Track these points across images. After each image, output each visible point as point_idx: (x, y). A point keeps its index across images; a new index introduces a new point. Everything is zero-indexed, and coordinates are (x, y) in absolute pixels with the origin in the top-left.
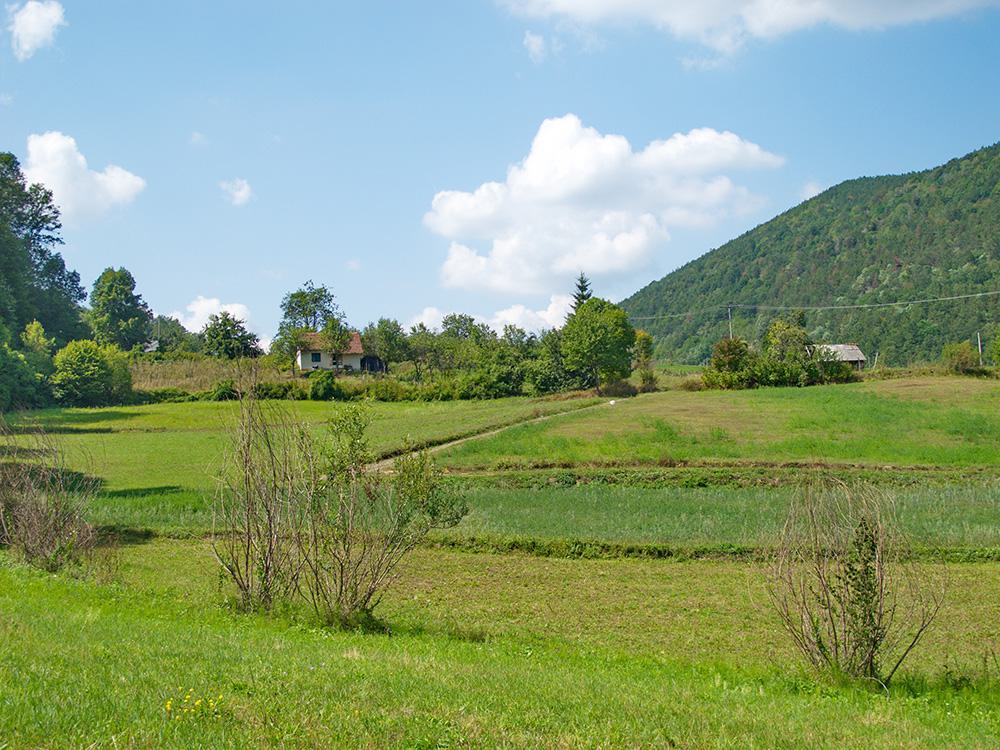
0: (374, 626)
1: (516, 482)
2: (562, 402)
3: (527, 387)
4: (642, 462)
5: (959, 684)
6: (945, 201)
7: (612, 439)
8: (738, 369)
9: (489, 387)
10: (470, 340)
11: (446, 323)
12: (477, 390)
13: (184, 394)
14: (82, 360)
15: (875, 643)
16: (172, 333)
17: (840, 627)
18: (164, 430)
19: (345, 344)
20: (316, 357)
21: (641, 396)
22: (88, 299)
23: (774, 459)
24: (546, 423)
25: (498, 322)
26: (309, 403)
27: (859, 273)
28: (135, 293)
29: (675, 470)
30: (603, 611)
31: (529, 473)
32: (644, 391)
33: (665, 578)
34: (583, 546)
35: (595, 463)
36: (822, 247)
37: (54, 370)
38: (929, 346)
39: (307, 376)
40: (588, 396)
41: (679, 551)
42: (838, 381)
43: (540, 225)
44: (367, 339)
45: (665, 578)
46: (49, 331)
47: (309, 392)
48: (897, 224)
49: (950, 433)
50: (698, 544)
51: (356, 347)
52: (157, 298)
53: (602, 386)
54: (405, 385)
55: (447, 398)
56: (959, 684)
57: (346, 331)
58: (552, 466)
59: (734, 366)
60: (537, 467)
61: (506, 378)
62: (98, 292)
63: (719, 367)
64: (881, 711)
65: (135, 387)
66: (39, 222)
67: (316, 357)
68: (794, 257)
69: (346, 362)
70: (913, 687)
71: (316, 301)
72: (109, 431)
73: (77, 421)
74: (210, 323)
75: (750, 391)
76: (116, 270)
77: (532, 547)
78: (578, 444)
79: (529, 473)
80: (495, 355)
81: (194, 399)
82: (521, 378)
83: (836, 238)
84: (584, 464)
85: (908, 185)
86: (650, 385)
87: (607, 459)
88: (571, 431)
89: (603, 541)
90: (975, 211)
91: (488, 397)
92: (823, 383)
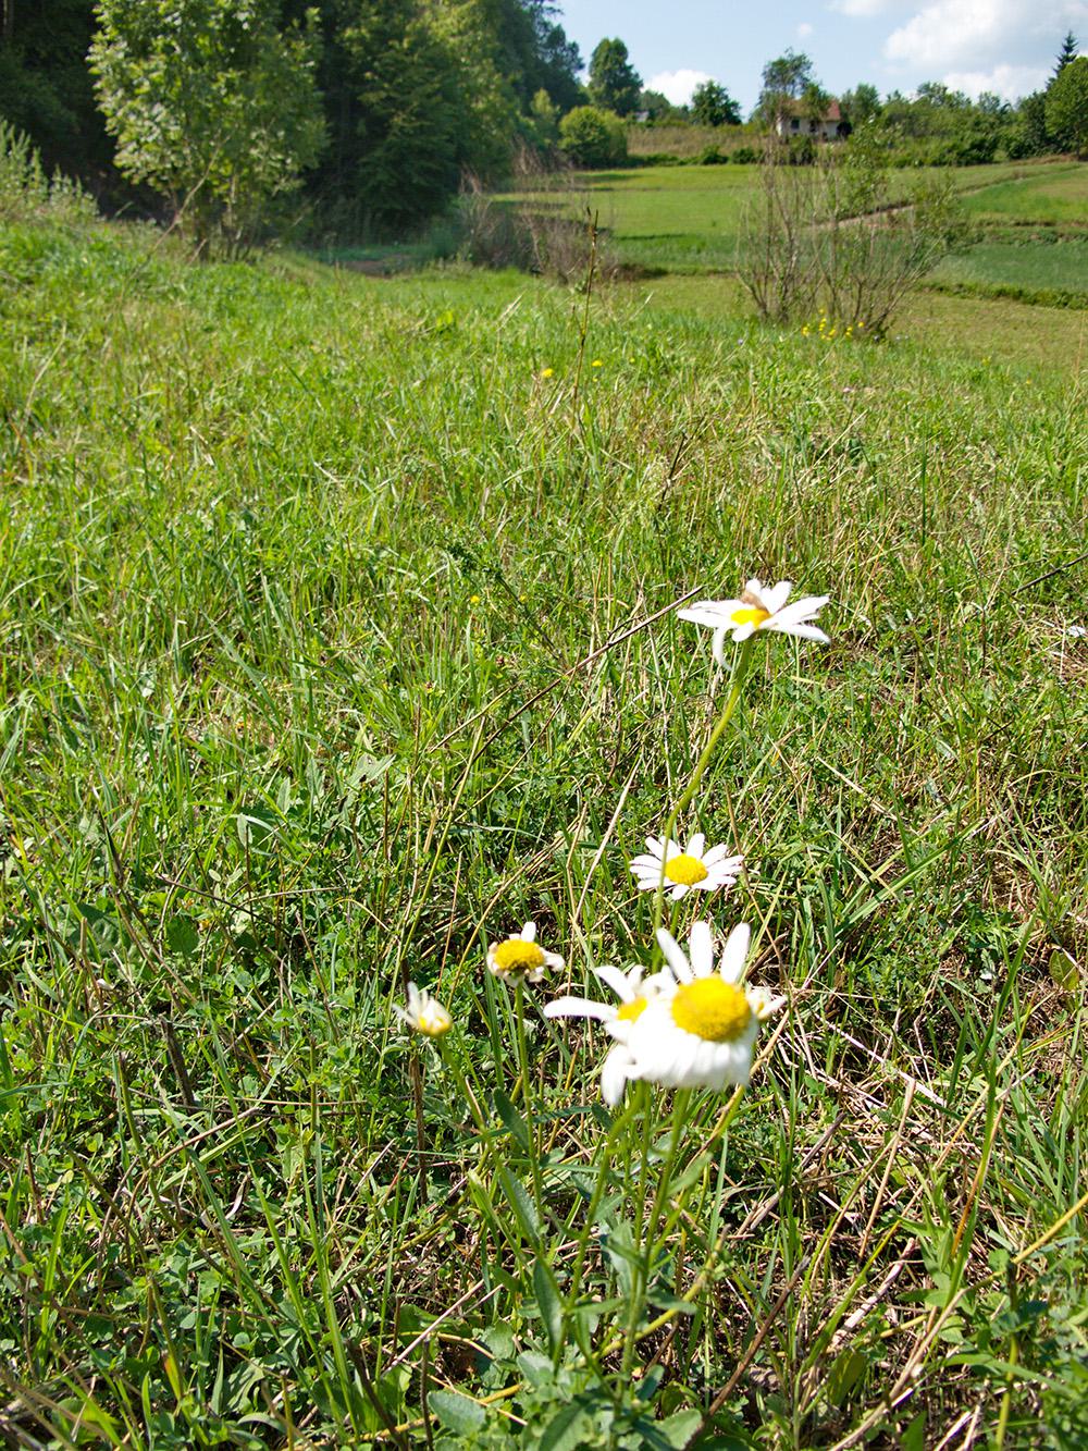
1: (998, 238)
3: (1000, 154)
9: (962, 154)
10: (944, 108)
11: (920, 92)
12: (948, 157)
13: (674, 159)
14: (584, 125)
16: (658, 106)
18: (658, 189)
19: (823, 110)
22: (587, 69)
24: (1027, 184)
25: (971, 87)
31: (1011, 230)
34: (1070, 297)
37: (560, 136)
40: (1067, 161)
44: (845, 107)
46: (554, 102)
51: (834, 114)
58: (1033, 224)
60: (1018, 224)
61: (979, 146)
62: (595, 64)
65: (630, 152)
67: (795, 124)
71: (796, 68)
72: (635, 177)
74: (697, 92)
77: (1018, 296)
79: (1011, 230)
80: (970, 121)
81: (682, 164)
82: (994, 146)
84: (1066, 222)
88: (1054, 191)
91: (959, 164)
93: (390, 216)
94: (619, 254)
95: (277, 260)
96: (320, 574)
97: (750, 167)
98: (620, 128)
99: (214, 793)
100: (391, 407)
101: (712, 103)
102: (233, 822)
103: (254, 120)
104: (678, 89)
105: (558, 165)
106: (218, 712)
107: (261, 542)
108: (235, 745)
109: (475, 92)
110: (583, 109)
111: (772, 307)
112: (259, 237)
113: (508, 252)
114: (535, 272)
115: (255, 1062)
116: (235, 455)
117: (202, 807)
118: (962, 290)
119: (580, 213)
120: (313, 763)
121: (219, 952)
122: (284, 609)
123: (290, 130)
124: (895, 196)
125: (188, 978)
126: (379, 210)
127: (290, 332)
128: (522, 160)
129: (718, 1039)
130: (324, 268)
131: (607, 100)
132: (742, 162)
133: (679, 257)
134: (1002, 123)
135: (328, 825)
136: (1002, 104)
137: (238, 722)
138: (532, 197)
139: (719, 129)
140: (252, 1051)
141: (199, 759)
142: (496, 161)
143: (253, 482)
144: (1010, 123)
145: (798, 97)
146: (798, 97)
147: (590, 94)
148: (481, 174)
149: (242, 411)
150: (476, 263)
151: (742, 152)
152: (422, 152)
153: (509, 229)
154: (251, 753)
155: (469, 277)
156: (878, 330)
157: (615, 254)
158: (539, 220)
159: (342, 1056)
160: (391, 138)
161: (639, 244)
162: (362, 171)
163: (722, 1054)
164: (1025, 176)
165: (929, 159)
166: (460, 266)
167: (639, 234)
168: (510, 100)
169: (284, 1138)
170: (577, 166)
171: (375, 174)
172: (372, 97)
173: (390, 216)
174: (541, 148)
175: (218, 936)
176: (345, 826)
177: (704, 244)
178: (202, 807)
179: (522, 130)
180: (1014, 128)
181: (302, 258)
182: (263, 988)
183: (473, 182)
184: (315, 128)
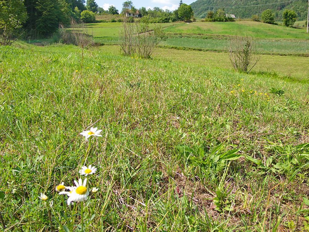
2: (178, 23)
3: (170, 21)
4: (195, 34)
8: (212, 18)
9: (163, 21)
10: (159, 12)
14: (86, 14)
15: (247, 65)
16: (102, 11)
18: (102, 27)
19: (136, 12)
20: (130, 14)
21: (193, 22)
22: (86, 3)
29: (201, 36)
34: (185, 48)
40: (183, 22)
41: (203, 50)
42: (231, 21)
44: (139, 11)
46: (79, 9)
49: (253, 32)
50: (207, 49)
51: (137, 13)
58: (178, 34)
59: (211, 17)
60: (175, 34)
61: (166, 19)
63: (208, 17)
67: (130, 14)
71: (129, 4)
75: (214, 22)
77: (176, 48)
81: (107, 22)
82: (169, 19)
86: (195, 20)
87: (188, 33)
88: (181, 28)
89: (189, 47)
91: (163, 23)
93: (43, 33)
94: (94, 41)
95: (17, 43)
96: (29, 118)
97: (121, 23)
98: (93, 15)
99: (7, 166)
100: (43, 79)
101: (113, 10)
102: (11, 171)
103: (10, 12)
104: (106, 8)
105: (80, 22)
106: (7, 149)
107: (15, 111)
108: (11, 156)
109: (62, 7)
110: (85, 11)
111: (127, 51)
112: (13, 38)
113: (70, 40)
114: (77, 45)
115: (19, 218)
116: (8, 92)
117: (5, 169)
118: (165, 47)
119: (86, 33)
120: (28, 158)
121: (10, 197)
122: (21, 125)
123: (18, 15)
124: (150, 29)
125: (3, 203)
126: (41, 32)
127: (20, 62)
128: (72, 22)
129: (82, 194)
130: (28, 44)
131: (90, 9)
132: (119, 22)
133: (107, 41)
134: (170, 15)
135: (31, 170)
136: (170, 11)
137: (12, 151)
138: (75, 29)
140: (17, 216)
141: (3, 159)
142: (67, 21)
143: (13, 98)
144: (172, 15)
145: (130, 9)
146: (130, 9)
147: (87, 8)
148: (63, 24)
149: (9, 81)
150: (63, 43)
152: (50, 19)
153: (71, 36)
154: (15, 157)
155: (62, 46)
156: (148, 55)
157: (94, 41)
158: (77, 34)
159: (34, 210)
160: (43, 16)
161: (99, 39)
162: (36, 23)
163: (83, 196)
164: (175, 25)
165: (157, 22)
166: (60, 44)
167: (98, 37)
168: (69, 9)
169: (24, 228)
170: (84, 23)
171: (40, 24)
172: (38, 7)
173: (43, 33)
174: (76, 19)
175: (9, 194)
176: (35, 170)
177: (112, 39)
178: (5, 169)
179: (72, 15)
180: (173, 16)
181: (23, 42)
182: (19, 203)
183: (62, 26)
184: (25, 15)
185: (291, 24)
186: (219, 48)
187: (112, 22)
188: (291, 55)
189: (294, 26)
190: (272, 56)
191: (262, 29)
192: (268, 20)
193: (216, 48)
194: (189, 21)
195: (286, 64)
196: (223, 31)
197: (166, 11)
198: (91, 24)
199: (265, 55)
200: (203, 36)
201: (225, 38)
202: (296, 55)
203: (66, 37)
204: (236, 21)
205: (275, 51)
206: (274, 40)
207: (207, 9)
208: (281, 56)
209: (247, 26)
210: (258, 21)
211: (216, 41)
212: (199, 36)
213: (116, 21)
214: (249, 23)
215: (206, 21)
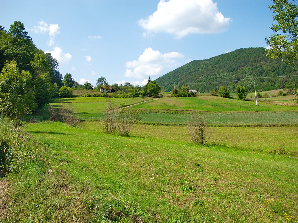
0: (128, 136)
1: (142, 113)
2: (147, 99)
3: (140, 95)
4: (162, 110)
5: (215, 145)
6: (211, 65)
7: (157, 106)
8: (177, 94)
9: (134, 95)
12: (131, 96)
13: (81, 96)
14: (64, 90)
15: (203, 139)
17: (198, 137)
18: (80, 102)
19: (109, 88)
20: (104, 90)
21: (161, 98)
23: (184, 110)
25: (135, 84)
26: (103, 98)
27: (196, 76)
28: (71, 78)
29: (169, 112)
30: (160, 134)
32: (161, 97)
33: (168, 129)
34: (155, 124)
35: (155, 110)
36: (189, 72)
38: (207, 90)
39: (102, 93)
40: (151, 98)
41: (170, 125)
42: (193, 96)
43: (143, 68)
44: (113, 86)
45: (168, 129)
47: (103, 96)
48: (202, 68)
49: (212, 106)
50: (173, 123)
52: (74, 78)
53: (154, 96)
54: (119, 95)
55: (126, 97)
56: (215, 145)
57: (109, 85)
59: (176, 93)
61: (137, 94)
63: (174, 93)
64: (204, 148)
65: (73, 95)
66: (55, 65)
67: (104, 90)
68: (185, 73)
69: (109, 91)
70: (208, 145)
71: (103, 80)
72: (70, 102)
73: (65, 100)
75: (179, 98)
76: (68, 74)
78: (151, 106)
80: (135, 90)
81: (83, 97)
82: (139, 94)
83: (192, 70)
85: (204, 62)
86: (162, 96)
87: (156, 109)
88: (150, 104)
89: (158, 123)
90: (215, 66)
92: (191, 96)
101: (88, 86)
110: (64, 87)
113: (58, 117)
114: (63, 122)
139: (89, 90)
147: (64, 83)
150: (52, 120)
151: (94, 95)
165: (128, 96)
185: (244, 98)
186: (182, 123)
187: (88, 97)
188: (242, 126)
189: (246, 99)
190: (226, 128)
191: (220, 102)
192: (225, 95)
193: (181, 122)
194: (157, 97)
195: (237, 135)
196: (187, 105)
197: (136, 86)
198: (69, 98)
199: (220, 127)
200: (170, 112)
201: (188, 112)
202: (246, 126)
203: (54, 114)
204: (198, 96)
205: (229, 123)
206: (229, 112)
207: (172, 82)
208: (234, 128)
209: (206, 101)
210: (217, 96)
211: (181, 115)
212: (166, 111)
213: (91, 96)
214: (209, 98)
215: (172, 96)
